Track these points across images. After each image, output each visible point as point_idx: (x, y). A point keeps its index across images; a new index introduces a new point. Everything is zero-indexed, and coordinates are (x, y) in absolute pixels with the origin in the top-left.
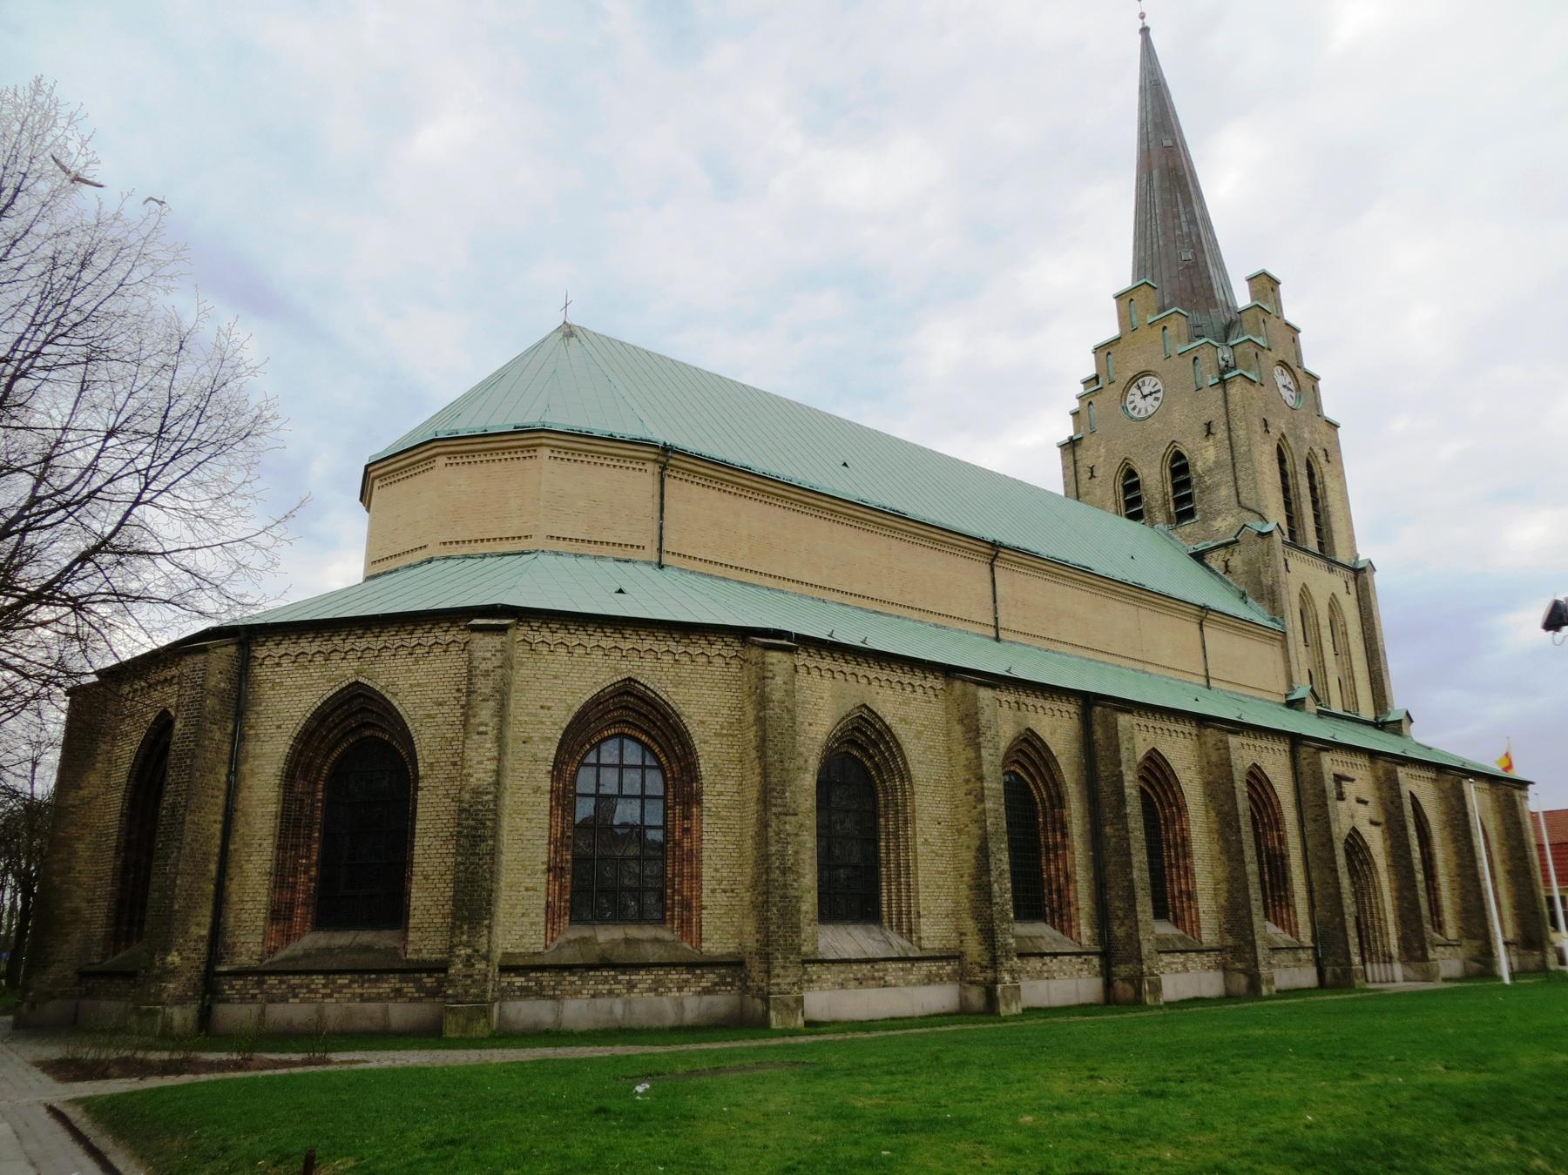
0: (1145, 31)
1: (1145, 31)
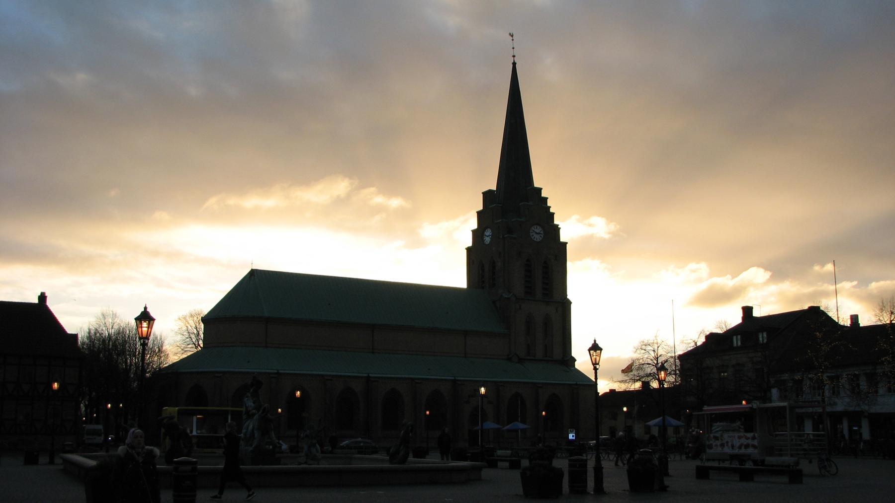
0: (514, 64)
1: (514, 64)
